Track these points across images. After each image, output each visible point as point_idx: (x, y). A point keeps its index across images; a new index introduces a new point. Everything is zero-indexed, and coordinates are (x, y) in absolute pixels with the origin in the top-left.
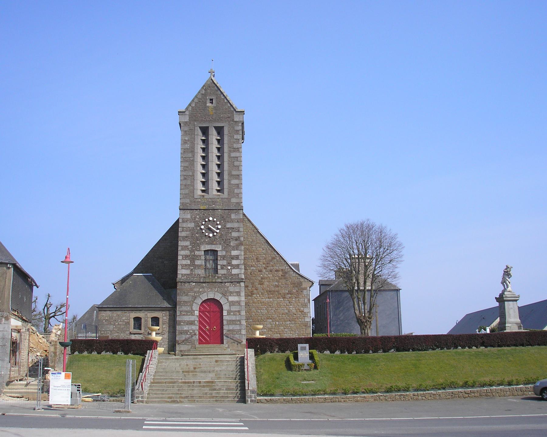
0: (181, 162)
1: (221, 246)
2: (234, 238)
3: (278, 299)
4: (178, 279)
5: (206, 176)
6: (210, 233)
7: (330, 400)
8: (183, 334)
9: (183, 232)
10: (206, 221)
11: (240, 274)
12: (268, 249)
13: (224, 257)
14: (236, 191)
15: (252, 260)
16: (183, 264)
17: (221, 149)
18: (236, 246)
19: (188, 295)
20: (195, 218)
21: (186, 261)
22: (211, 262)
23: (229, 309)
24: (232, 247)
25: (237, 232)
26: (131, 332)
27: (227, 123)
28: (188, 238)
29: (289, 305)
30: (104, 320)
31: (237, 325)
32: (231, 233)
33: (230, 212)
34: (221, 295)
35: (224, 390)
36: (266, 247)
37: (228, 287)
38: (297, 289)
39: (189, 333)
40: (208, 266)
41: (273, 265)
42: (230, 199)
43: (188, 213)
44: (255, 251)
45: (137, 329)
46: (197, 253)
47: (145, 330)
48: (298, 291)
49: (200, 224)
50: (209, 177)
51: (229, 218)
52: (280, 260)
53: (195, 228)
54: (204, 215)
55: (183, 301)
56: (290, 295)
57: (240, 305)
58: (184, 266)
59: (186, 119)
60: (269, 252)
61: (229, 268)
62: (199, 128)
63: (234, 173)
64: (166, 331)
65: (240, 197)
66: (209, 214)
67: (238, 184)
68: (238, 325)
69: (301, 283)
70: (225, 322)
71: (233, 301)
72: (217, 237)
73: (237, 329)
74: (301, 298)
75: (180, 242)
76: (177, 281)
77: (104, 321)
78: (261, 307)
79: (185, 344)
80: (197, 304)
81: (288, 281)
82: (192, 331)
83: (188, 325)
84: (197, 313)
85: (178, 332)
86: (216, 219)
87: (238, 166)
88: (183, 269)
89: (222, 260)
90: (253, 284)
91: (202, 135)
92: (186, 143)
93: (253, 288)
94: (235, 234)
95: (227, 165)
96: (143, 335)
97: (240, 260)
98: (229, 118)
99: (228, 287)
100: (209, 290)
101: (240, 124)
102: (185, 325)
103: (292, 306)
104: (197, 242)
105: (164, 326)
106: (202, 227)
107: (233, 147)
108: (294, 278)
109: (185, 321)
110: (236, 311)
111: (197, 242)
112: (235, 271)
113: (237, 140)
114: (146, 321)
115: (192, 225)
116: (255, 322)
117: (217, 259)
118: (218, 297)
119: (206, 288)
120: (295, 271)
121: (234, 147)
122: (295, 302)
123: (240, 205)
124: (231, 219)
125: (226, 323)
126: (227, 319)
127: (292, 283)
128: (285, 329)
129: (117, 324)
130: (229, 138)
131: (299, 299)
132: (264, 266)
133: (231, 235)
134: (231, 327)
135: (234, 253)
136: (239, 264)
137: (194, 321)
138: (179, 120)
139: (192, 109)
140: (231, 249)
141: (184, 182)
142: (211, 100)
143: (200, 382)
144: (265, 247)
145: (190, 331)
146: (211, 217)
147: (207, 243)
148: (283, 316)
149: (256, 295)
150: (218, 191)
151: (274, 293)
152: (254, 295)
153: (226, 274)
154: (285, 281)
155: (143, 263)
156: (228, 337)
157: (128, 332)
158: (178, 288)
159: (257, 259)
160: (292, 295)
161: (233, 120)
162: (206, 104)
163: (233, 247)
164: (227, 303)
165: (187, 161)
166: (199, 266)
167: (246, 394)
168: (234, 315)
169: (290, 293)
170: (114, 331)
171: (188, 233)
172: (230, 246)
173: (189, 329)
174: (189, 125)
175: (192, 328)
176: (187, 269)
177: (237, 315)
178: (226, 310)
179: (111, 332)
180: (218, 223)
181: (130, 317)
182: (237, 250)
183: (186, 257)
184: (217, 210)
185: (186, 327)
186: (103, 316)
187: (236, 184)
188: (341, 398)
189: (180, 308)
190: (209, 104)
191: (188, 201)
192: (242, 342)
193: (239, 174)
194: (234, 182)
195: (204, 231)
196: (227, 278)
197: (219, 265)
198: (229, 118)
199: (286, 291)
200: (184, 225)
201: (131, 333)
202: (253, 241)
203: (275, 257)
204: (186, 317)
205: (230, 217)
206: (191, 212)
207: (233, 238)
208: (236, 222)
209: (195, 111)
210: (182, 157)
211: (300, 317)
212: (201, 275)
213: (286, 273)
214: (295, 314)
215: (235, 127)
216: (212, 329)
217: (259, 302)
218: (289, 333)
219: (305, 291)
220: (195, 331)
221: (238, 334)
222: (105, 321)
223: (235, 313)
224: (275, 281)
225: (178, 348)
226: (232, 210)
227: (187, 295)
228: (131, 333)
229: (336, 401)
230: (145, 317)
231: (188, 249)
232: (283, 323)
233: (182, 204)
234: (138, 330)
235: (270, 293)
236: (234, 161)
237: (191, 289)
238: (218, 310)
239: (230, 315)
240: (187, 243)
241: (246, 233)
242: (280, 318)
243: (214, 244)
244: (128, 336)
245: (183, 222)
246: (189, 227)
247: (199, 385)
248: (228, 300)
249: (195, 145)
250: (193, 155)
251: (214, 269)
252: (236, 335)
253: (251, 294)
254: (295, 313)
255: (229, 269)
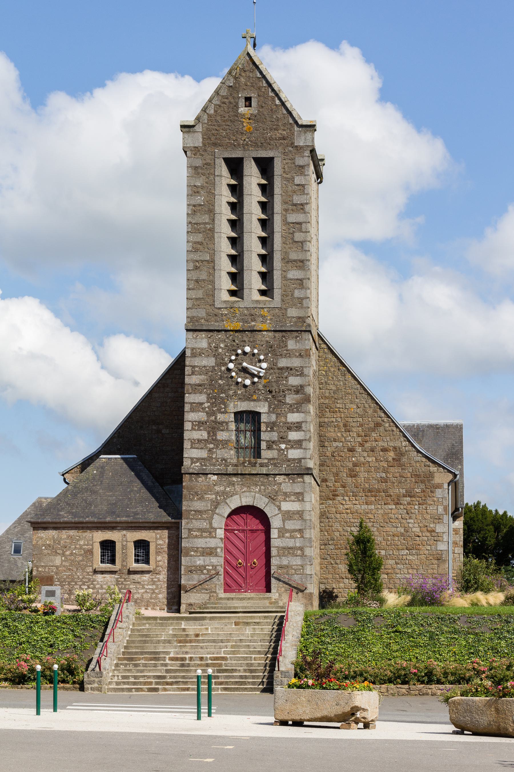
0: (188, 232)
1: (267, 404)
2: (293, 388)
3: (386, 506)
4: (184, 468)
5: (238, 261)
6: (246, 379)
7: (418, 691)
8: (194, 572)
9: (193, 376)
10: (237, 355)
11: (304, 459)
12: (367, 406)
13: (272, 426)
14: (297, 293)
15: (336, 429)
16: (194, 439)
17: (268, 204)
18: (296, 404)
19: (204, 498)
20: (217, 347)
21: (200, 434)
22: (248, 434)
23: (283, 527)
24: (288, 406)
25: (299, 377)
26: (95, 569)
27: (280, 149)
28: (203, 387)
29: (408, 518)
30: (44, 545)
31: (296, 556)
32: (286, 378)
33: (284, 337)
34: (267, 500)
35: (242, 671)
36: (364, 402)
37: (281, 484)
38: (422, 486)
39: (205, 571)
40: (242, 443)
41: (376, 438)
42: (286, 309)
43: (202, 339)
44: (341, 410)
45: (108, 563)
46: (220, 417)
47: (122, 565)
48: (424, 491)
49: (226, 359)
50: (245, 265)
51: (284, 349)
52: (390, 428)
53: (216, 368)
54: (234, 341)
55: (194, 511)
56: (408, 499)
57: (302, 519)
58: (197, 443)
59: (197, 140)
60: (370, 412)
61: (283, 446)
62: (223, 160)
63: (293, 256)
64: (162, 568)
65: (305, 305)
66: (243, 339)
67: (301, 280)
68: (299, 557)
69: (431, 475)
70: (274, 552)
71: (289, 512)
72: (260, 387)
73: (297, 565)
74: (431, 505)
75: (187, 395)
76: (183, 472)
77: (44, 548)
78: (352, 520)
79: (197, 592)
80: (221, 515)
81: (407, 471)
82: (211, 568)
83: (203, 556)
84: (220, 533)
85: (185, 569)
86: (258, 351)
87: (302, 243)
88: (194, 448)
89: (269, 431)
90: (336, 475)
91: (230, 176)
92: (198, 192)
93: (336, 484)
94: (294, 381)
95: (280, 239)
96: (120, 573)
97: (303, 431)
98: (284, 139)
99: (281, 484)
100: (243, 490)
101: (307, 153)
102: (199, 556)
103: (412, 521)
104: (221, 395)
105: (159, 558)
106: (231, 366)
107: (293, 200)
108: (418, 465)
109: (197, 548)
110: (294, 530)
111: (221, 395)
112: (294, 454)
113: (301, 187)
114: (124, 547)
115: (211, 362)
116: (339, 550)
117: (259, 430)
118: (261, 502)
119: (238, 485)
120: (420, 450)
121: (295, 202)
122: (419, 512)
123: (305, 322)
124: (287, 350)
125: (276, 552)
126: (277, 545)
127: (414, 475)
128: (398, 565)
129: (68, 553)
130: (285, 182)
131: (426, 507)
132: (360, 439)
133: (287, 381)
134: (285, 561)
135: (293, 417)
136: (301, 439)
137: (216, 548)
138: (184, 144)
139: (208, 120)
140: (286, 409)
141: (195, 275)
142: (248, 100)
143: (201, 659)
144: (361, 402)
145: (207, 567)
146: (248, 346)
147: (240, 399)
148: (393, 540)
149: (342, 498)
150: (263, 293)
151: (378, 494)
152: (339, 498)
153: (277, 459)
154: (400, 470)
155: (119, 433)
156: (279, 580)
157: (90, 569)
158: (184, 484)
159: (345, 425)
160: (413, 499)
161: (293, 143)
162: (238, 108)
163: (291, 406)
164: (278, 514)
165: (198, 231)
166: (225, 443)
167: (275, 678)
168: (292, 537)
169: (410, 494)
170: (64, 566)
171: (203, 377)
172: (285, 403)
173: (206, 564)
174: (202, 155)
175: (212, 561)
176: (202, 448)
177: (297, 538)
178: (277, 528)
179: (57, 569)
180: (262, 357)
181: (92, 540)
182: (298, 412)
183: (199, 425)
184: (260, 333)
185: (200, 560)
186: (42, 538)
187: (297, 279)
188: (437, 689)
189: (188, 523)
190: (243, 110)
191: (201, 313)
192: (306, 588)
193: (303, 259)
194: (294, 275)
195: (234, 374)
196: (277, 466)
197: (264, 440)
198: (284, 139)
199: (401, 490)
200: (198, 362)
201: (95, 572)
202: (338, 389)
203: (381, 422)
204: (200, 540)
205: (286, 346)
206: (209, 336)
207: (290, 387)
208: (297, 357)
209: (215, 123)
210: (190, 223)
211: (428, 542)
212: (228, 461)
213: (402, 454)
214: (419, 536)
215: (297, 158)
216: (249, 564)
217: (349, 511)
218: (406, 573)
219: (440, 490)
220: (217, 567)
221: (298, 574)
222: (45, 547)
223: (293, 534)
224: (381, 471)
225: (186, 599)
226: (289, 333)
227: (202, 498)
228: (95, 572)
229: (427, 694)
230: (122, 540)
231: (204, 409)
232: (395, 553)
233: (191, 319)
234: (109, 565)
235: (369, 494)
236: (294, 232)
237: (209, 489)
238: (261, 527)
239: (283, 537)
240: (202, 398)
241: (324, 373)
242: (389, 543)
243: (254, 400)
244: (91, 577)
245: (194, 355)
246: (205, 367)
247: (199, 662)
248: (280, 509)
249: (216, 197)
250: (212, 218)
251: (255, 448)
252: (295, 575)
253: (333, 495)
254: (417, 534)
255: (282, 450)
